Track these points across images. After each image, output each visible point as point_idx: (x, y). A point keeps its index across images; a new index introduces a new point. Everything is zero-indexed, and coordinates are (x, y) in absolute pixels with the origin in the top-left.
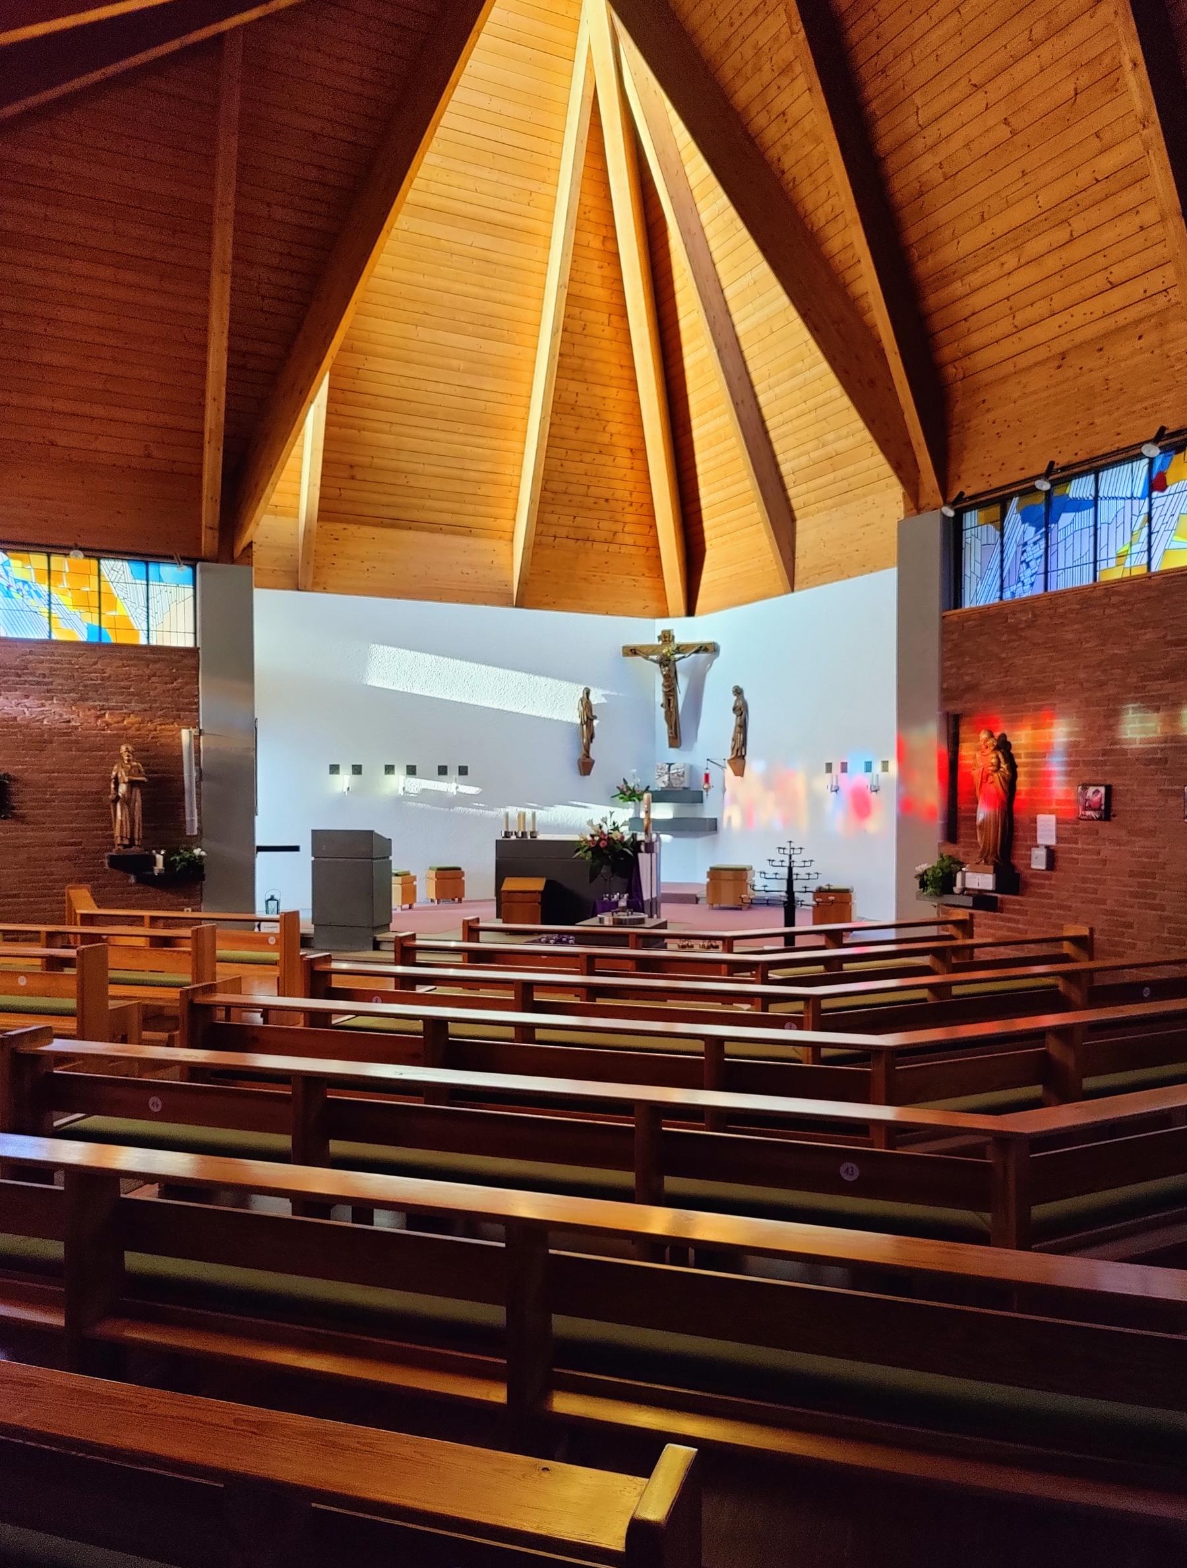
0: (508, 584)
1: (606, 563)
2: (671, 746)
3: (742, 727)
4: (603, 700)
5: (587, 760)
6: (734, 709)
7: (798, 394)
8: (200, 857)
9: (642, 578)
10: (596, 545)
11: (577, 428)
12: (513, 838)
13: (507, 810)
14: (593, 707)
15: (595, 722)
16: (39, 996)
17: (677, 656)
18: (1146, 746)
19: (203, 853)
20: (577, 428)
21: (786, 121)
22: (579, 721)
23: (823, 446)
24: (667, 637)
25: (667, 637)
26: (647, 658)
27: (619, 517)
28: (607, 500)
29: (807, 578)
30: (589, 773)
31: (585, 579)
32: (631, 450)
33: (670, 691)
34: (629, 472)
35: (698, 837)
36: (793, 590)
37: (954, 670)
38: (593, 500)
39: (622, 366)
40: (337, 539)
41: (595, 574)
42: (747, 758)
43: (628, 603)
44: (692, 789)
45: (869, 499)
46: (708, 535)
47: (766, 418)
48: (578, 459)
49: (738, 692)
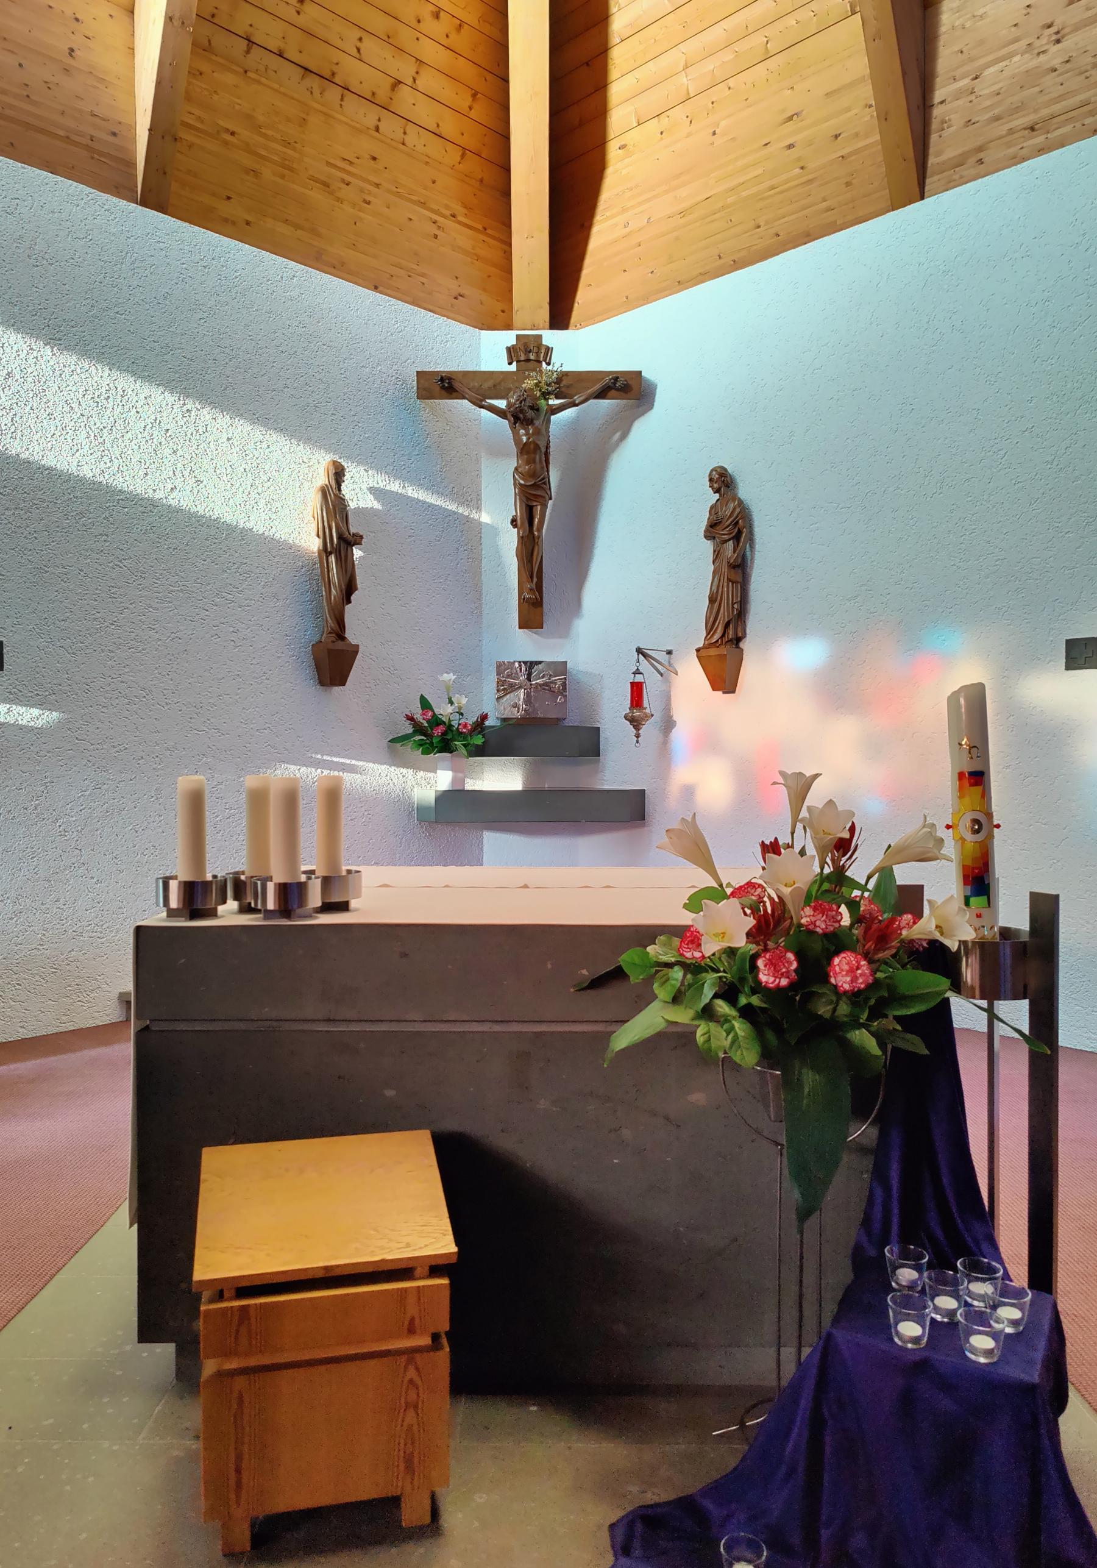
0: (122, 131)
1: (374, 159)
2: (524, 624)
4: (370, 502)
5: (340, 645)
9: (449, 223)
10: (352, 104)
12: (229, 914)
13: (453, 707)
15: (357, 553)
16: (480, 599)
17: (554, 402)
22: (314, 544)
27: (405, 36)
29: (980, 149)
31: (326, 185)
35: (581, 832)
36: (922, 198)
41: (348, 178)
42: (745, 645)
43: (423, 275)
44: (567, 723)
49: (722, 481)
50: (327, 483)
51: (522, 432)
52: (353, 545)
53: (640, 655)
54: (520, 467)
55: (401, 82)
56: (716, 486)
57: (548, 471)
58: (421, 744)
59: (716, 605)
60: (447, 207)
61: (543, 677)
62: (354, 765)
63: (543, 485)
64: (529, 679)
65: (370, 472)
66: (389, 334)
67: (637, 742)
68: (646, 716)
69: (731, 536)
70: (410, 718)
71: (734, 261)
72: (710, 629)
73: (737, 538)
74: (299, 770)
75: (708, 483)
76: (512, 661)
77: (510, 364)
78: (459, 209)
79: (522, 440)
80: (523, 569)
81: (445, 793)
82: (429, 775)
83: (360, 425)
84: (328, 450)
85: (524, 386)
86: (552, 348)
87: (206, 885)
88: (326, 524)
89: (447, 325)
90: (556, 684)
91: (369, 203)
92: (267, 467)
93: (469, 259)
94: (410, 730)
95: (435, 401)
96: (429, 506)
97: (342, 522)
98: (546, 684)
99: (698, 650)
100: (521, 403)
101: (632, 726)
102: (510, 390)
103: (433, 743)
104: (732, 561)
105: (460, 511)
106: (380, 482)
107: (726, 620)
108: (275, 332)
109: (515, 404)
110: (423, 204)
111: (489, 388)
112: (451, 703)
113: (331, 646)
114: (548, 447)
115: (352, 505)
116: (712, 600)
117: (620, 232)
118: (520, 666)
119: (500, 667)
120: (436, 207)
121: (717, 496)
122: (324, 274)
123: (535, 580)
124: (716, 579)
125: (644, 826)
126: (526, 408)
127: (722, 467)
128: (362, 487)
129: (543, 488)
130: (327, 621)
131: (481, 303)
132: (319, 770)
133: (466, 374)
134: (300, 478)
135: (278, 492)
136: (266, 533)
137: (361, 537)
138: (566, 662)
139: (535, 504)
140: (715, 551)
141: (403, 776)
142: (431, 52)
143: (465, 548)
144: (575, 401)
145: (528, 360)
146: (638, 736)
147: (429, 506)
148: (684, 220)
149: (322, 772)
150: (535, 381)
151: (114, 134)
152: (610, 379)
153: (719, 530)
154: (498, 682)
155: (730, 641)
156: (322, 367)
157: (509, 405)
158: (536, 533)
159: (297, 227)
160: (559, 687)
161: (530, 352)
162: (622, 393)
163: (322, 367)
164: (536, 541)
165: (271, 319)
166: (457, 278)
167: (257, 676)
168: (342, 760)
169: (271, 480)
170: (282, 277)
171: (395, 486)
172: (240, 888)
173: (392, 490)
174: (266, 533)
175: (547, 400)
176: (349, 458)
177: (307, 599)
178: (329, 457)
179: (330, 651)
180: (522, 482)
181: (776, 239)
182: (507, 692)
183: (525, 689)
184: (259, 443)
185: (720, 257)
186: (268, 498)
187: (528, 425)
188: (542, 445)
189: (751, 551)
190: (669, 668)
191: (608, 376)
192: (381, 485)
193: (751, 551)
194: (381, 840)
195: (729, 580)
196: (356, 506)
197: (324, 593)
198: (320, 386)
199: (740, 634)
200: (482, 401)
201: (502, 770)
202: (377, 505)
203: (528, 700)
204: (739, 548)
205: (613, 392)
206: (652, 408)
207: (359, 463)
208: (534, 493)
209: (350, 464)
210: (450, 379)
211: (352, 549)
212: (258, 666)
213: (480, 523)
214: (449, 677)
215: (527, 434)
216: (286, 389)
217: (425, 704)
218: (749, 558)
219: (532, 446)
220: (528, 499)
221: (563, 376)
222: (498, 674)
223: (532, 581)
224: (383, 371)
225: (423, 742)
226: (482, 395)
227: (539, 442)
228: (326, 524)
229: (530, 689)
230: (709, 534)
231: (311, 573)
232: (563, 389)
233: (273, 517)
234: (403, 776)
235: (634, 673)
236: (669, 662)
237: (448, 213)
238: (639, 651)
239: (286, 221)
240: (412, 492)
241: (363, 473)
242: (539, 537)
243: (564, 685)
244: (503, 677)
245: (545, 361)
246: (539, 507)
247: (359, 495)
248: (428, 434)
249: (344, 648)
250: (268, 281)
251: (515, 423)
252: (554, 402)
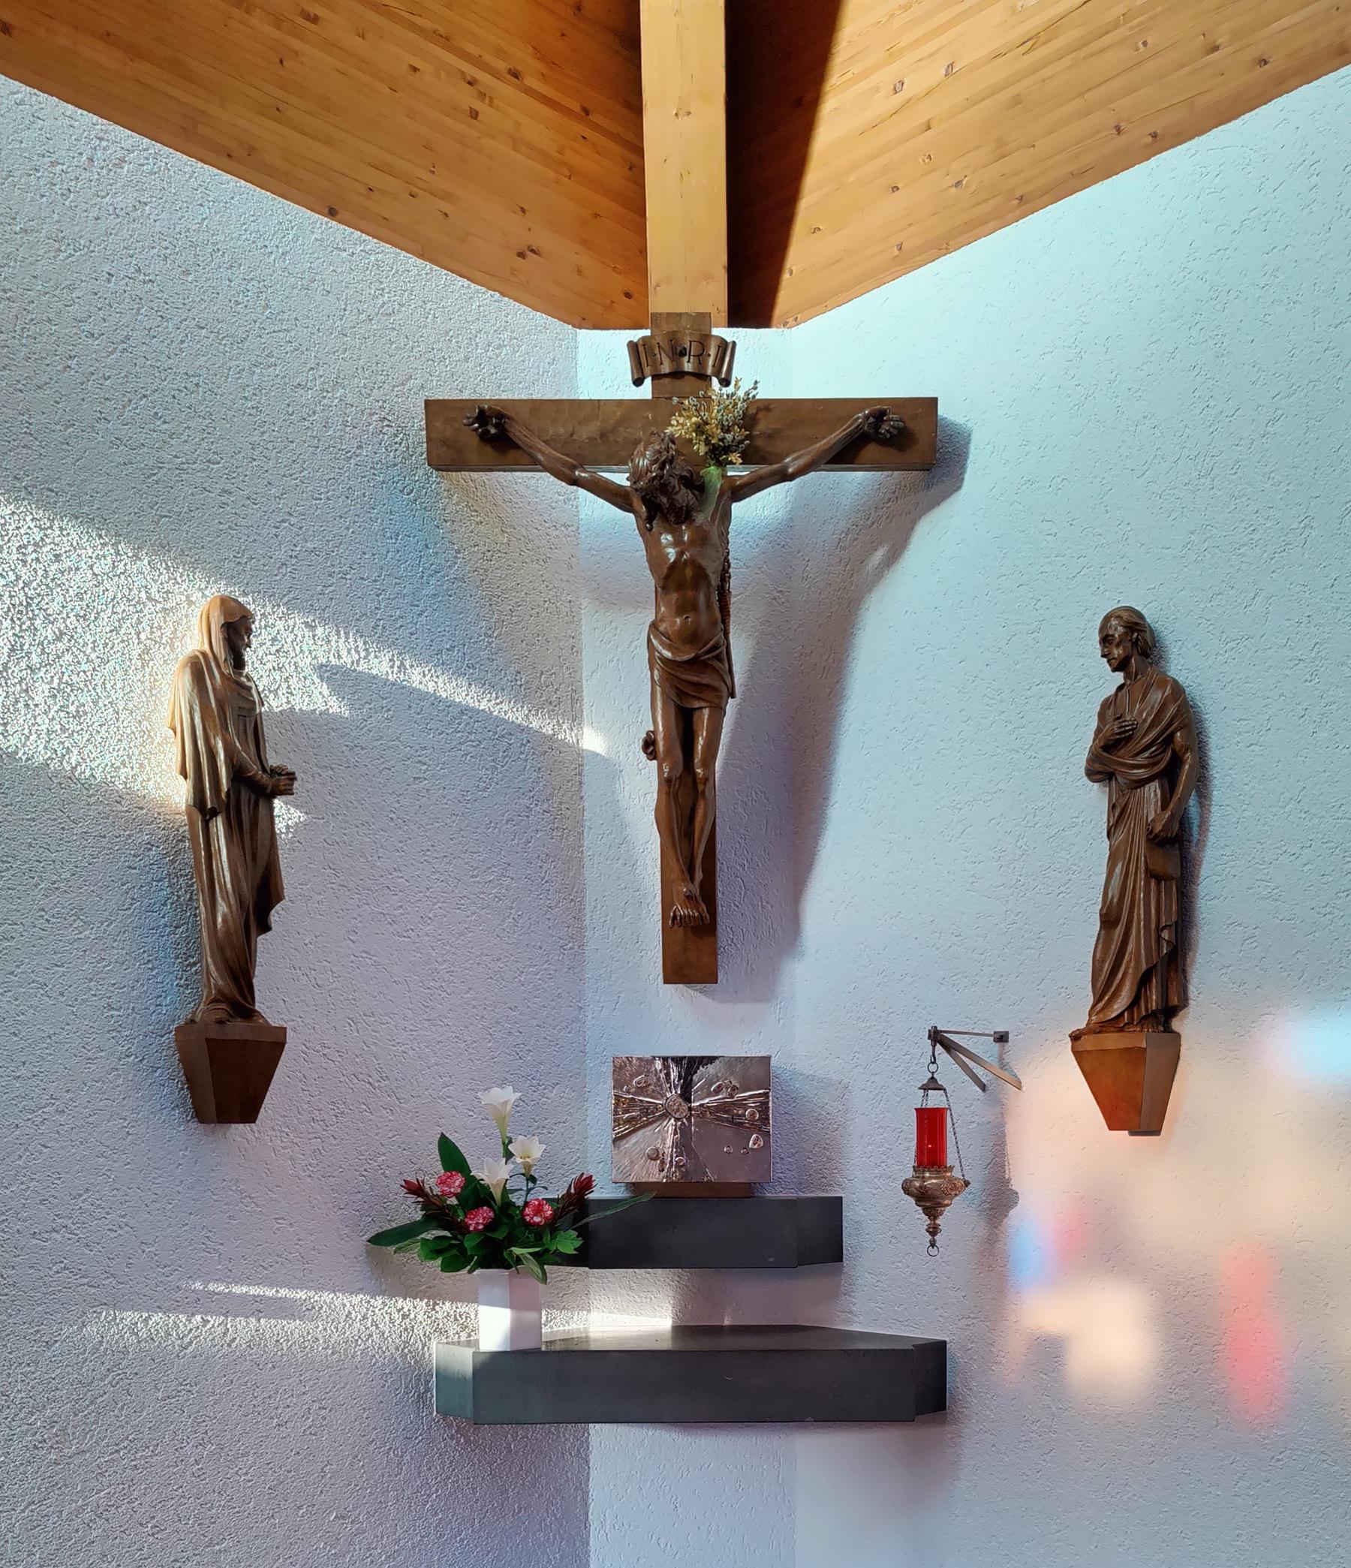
9: (505, 90)
13: (511, 1166)
14: (269, 731)
15: (285, 814)
16: (579, 918)
18: (235, 840)
22: (179, 793)
30: (248, 1111)
33: (694, 663)
42: (1184, 1024)
43: (446, 196)
44: (775, 1192)
50: (206, 648)
51: (666, 538)
52: (274, 794)
53: (938, 1045)
54: (662, 621)
56: (1117, 652)
57: (726, 634)
58: (436, 1250)
59: (1119, 931)
60: (500, 53)
61: (718, 1091)
62: (285, 1299)
63: (716, 663)
64: (686, 1095)
65: (319, 631)
66: (363, 317)
67: (933, 1244)
68: (955, 1188)
69: (1157, 769)
70: (415, 1189)
71: (1154, 136)
72: (1104, 988)
73: (1169, 776)
74: (146, 1320)
75: (1097, 650)
76: (648, 1056)
77: (638, 382)
78: (524, 58)
79: (666, 556)
80: (671, 852)
81: (496, 1356)
82: (463, 1308)
83: (293, 520)
84: (215, 571)
85: (669, 430)
86: (734, 343)
88: (201, 743)
89: (500, 310)
90: (745, 1107)
91: (315, 19)
92: (54, 607)
93: (551, 174)
94: (418, 1215)
95: (474, 475)
96: (462, 713)
97: (244, 741)
98: (723, 1107)
99: (1075, 1037)
100: (662, 467)
101: (920, 1209)
102: (637, 442)
103: (466, 1249)
104: (1159, 827)
105: (535, 725)
106: (344, 653)
107: (1144, 967)
108: (72, 288)
109: (648, 470)
110: (445, 40)
111: (592, 439)
112: (508, 1155)
113: (214, 1033)
114: (724, 576)
115: (274, 704)
116: (1109, 920)
117: (885, 104)
118: (666, 1067)
119: (622, 1071)
120: (471, 48)
121: (1119, 678)
122: (200, 164)
123: (699, 876)
124: (1118, 870)
125: (943, 1422)
126: (675, 482)
127: (1130, 610)
128: (300, 664)
129: (714, 668)
130: (208, 973)
131: (579, 272)
132: (198, 1318)
133: (538, 406)
134: (143, 636)
135: (84, 667)
136: (54, 765)
137: (291, 777)
138: (768, 1059)
139: (697, 704)
140: (1112, 807)
141: (404, 1317)
143: (545, 806)
144: (786, 467)
146: (933, 1231)
147: (462, 713)
148: (1029, 59)
149: (205, 1322)
150: (694, 419)
152: (867, 417)
153: (1123, 755)
154: (617, 1105)
155: (1152, 1016)
156: (195, 380)
157: (635, 477)
158: (699, 771)
159: (134, 52)
160: (753, 1114)
161: (682, 354)
162: (891, 450)
163: (195, 380)
164: (700, 788)
165: (62, 256)
166: (523, 210)
167: (31, 1105)
168: (255, 1291)
169: (66, 638)
170: (91, 160)
171: (380, 665)
173: (374, 672)
174: (54, 765)
175: (722, 464)
176: (266, 593)
177: (163, 921)
178: (217, 589)
179: (214, 1046)
180: (668, 654)
181: (1259, 70)
182: (636, 1125)
183: (677, 1120)
184: (30, 548)
185: (1119, 130)
186: (56, 681)
187: (679, 522)
188: (712, 568)
189: (1201, 805)
190: (1000, 1073)
191: (862, 410)
192: (346, 660)
193: (1201, 805)
194: (351, 1464)
195: (1151, 874)
196: (285, 706)
197: (203, 909)
198: (192, 424)
199: (1175, 1001)
200: (574, 468)
201: (631, 1288)
202: (336, 706)
203: (683, 1144)
204: (1175, 799)
205: (872, 450)
206: (959, 487)
207: (293, 606)
208: (696, 679)
209: (269, 609)
210: (500, 416)
211: (271, 809)
212: (33, 1082)
213: (580, 753)
214: (504, 1096)
215: (677, 543)
216: (102, 425)
217: (451, 1156)
218: (1196, 823)
219: (689, 572)
220: (681, 694)
221: (759, 410)
222: (618, 1085)
223: (692, 879)
224: (349, 400)
225: (444, 1244)
226: (576, 456)
227: (704, 563)
228: (201, 743)
229: (689, 1120)
230: (1097, 766)
231: (173, 861)
232: (760, 442)
233: (73, 726)
234: (404, 1317)
235: (925, 1088)
236: (1001, 1059)
237: (502, 66)
238: (937, 1037)
239: (106, 36)
240: (422, 679)
241: (302, 632)
242: (706, 780)
243: (764, 1108)
244: (628, 1092)
245: (717, 374)
246: (706, 712)
247: (293, 682)
248: (458, 552)
249: (249, 1036)
250: (53, 164)
251: (650, 519)
252: (738, 471)
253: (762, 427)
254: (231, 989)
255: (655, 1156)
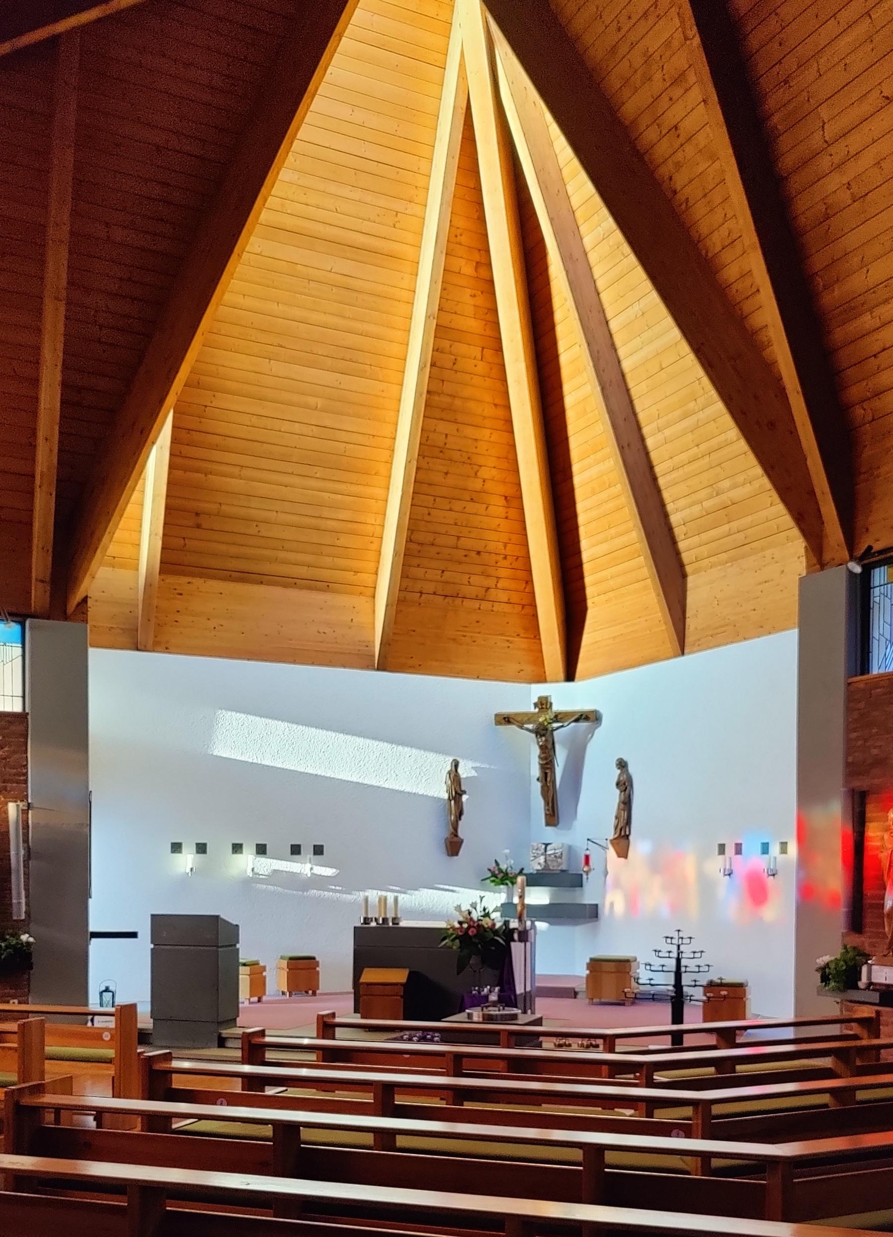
0: (369, 644)
2: (548, 824)
3: (627, 804)
4: (473, 773)
5: (455, 839)
6: (618, 784)
7: (690, 437)
8: (28, 943)
10: (467, 603)
11: (446, 473)
12: (373, 924)
13: (367, 894)
15: (465, 798)
17: (555, 725)
19: (31, 940)
20: (446, 473)
21: (678, 136)
22: (446, 796)
23: (717, 494)
24: (544, 704)
25: (544, 704)
26: (521, 727)
27: (491, 571)
28: (479, 553)
29: (699, 640)
31: (454, 640)
32: (506, 498)
33: (547, 764)
34: (503, 522)
37: (860, 743)
38: (463, 553)
39: (496, 405)
40: (181, 594)
41: (464, 634)
42: (631, 838)
45: (768, 553)
46: (590, 591)
47: (655, 463)
48: (448, 507)
49: (622, 765)
51: (540, 740)
55: (489, 588)
60: (514, 632)
87: (369, 919)
113: (451, 840)
116: (616, 818)
125: (597, 921)
142: (503, 573)
145: (542, 708)
151: (367, 646)
155: (623, 836)
172: (376, 920)
178: (451, 759)
210: (508, 718)
214: (507, 851)
253: (559, 717)
254: (454, 832)
255: (539, 864)
